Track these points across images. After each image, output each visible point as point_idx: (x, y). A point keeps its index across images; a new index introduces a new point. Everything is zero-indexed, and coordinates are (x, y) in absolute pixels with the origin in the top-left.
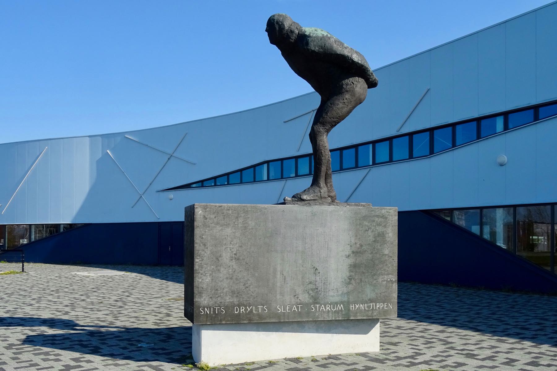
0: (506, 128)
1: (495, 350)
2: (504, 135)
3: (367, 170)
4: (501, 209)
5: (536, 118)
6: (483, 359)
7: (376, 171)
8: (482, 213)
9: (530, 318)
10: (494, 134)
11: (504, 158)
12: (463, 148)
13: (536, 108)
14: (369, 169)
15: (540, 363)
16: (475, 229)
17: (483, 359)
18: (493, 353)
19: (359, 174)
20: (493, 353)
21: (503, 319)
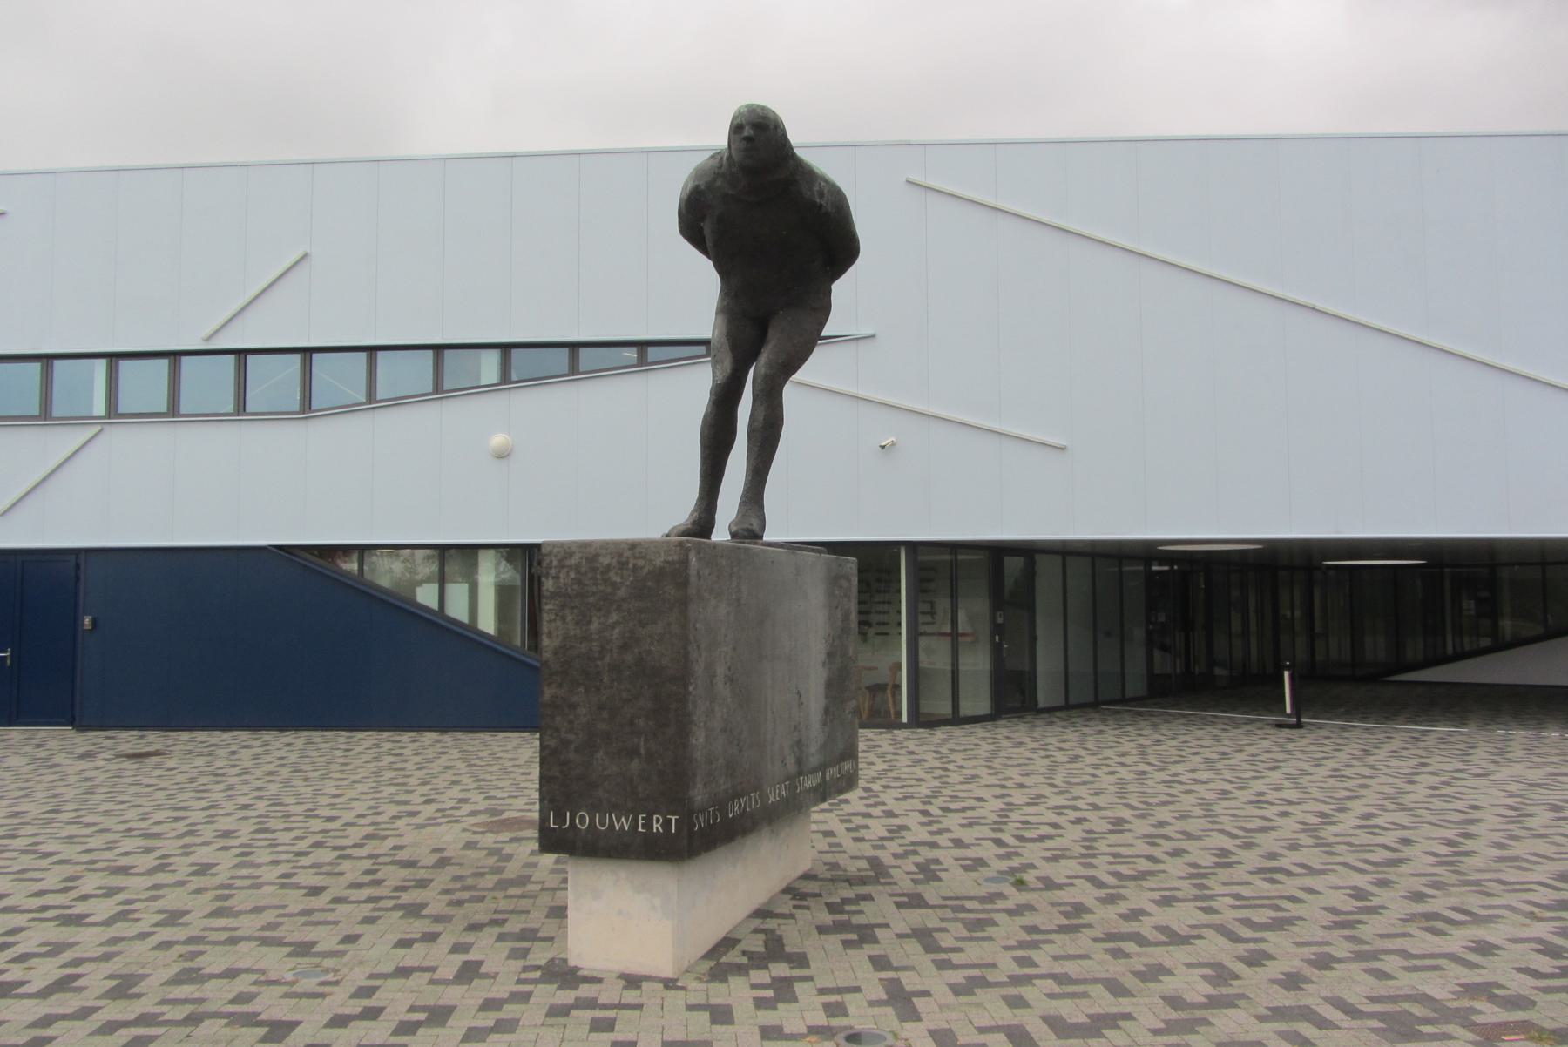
0: (505, 378)
1: (67, 956)
2: (436, 405)
3: (90, 432)
4: (492, 552)
5: (642, 360)
6: (44, 993)
7: (121, 438)
8: (455, 558)
9: (117, 836)
10: (475, 389)
11: (498, 440)
12: (415, 406)
13: (642, 345)
14: (98, 428)
15: (207, 971)
16: (427, 596)
17: (44, 993)
18: (64, 966)
19: (58, 442)
20: (64, 966)
21: (43, 848)
